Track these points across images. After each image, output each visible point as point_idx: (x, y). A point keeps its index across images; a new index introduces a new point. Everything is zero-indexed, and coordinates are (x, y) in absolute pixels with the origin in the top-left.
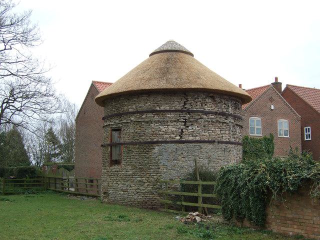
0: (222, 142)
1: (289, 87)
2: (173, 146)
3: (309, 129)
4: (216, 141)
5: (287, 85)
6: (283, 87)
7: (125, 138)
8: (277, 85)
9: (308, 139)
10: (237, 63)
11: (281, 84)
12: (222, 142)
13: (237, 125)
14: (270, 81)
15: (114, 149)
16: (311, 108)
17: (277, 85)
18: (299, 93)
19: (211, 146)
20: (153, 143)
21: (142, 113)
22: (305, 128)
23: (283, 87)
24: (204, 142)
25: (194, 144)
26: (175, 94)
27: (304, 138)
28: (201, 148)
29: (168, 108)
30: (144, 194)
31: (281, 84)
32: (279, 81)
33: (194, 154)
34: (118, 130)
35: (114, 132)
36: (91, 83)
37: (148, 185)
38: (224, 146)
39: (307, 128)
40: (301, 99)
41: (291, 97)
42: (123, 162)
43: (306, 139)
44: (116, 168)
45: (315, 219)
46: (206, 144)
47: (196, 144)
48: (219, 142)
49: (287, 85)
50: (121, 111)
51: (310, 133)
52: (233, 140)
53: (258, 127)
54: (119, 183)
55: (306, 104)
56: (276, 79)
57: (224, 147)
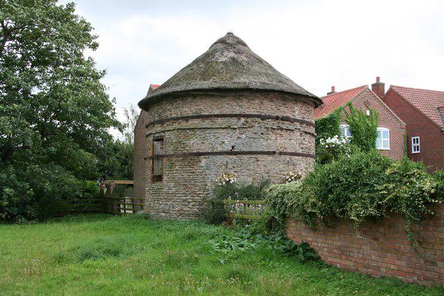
0: (286, 154)
1: (394, 88)
2: (225, 158)
3: (417, 139)
4: (278, 152)
5: (391, 86)
6: (386, 89)
7: (170, 150)
8: (378, 87)
9: (416, 152)
10: (320, 63)
11: (383, 85)
12: (286, 154)
13: (306, 133)
14: (370, 82)
15: (156, 162)
16: (421, 113)
17: (378, 87)
18: (406, 96)
19: (270, 158)
20: (199, 154)
21: (186, 119)
22: (413, 138)
23: (386, 89)
24: (298, 155)
25: (248, 156)
26: (296, 101)
27: (411, 151)
28: (258, 161)
29: (216, 112)
30: (188, 215)
31: (383, 85)
32: (381, 81)
33: (249, 167)
34: (160, 140)
35: (155, 143)
36: (149, 87)
37: (193, 205)
38: (287, 158)
39: (415, 138)
40: (408, 103)
41: (394, 100)
42: (165, 178)
43: (413, 152)
44: (158, 184)
45: (365, 247)
46: (265, 156)
47: (251, 156)
48: (280, 153)
49: (391, 86)
50: (164, 116)
51: (419, 144)
52: (300, 151)
53: (386, 139)
54: (161, 203)
55: (414, 109)
56: (378, 79)
57: (288, 159)
